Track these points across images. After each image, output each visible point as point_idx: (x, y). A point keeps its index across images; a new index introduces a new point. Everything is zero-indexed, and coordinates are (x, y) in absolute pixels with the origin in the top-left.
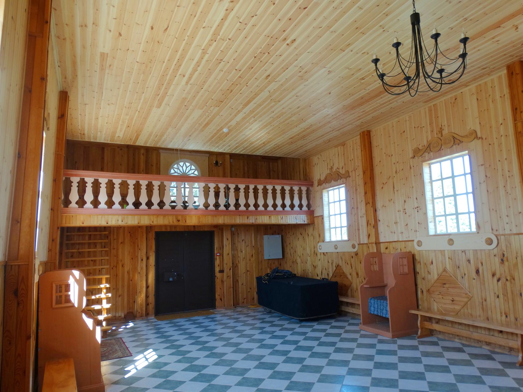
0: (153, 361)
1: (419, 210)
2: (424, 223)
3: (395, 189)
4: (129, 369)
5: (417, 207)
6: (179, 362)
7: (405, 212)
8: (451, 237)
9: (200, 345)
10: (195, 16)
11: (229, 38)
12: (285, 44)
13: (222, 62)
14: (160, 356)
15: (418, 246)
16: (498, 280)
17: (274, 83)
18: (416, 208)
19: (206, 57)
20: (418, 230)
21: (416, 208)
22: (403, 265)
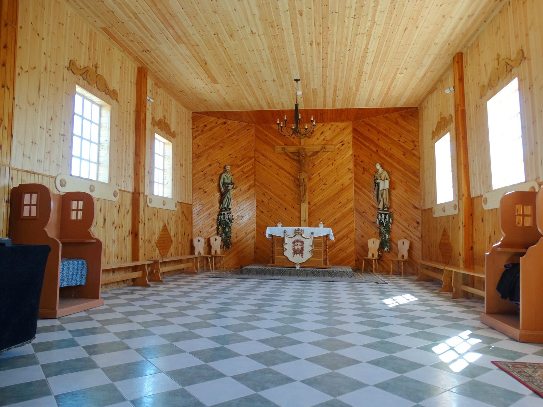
0: (438, 344)
1: (65, 139)
2: (67, 157)
3: (40, 92)
4: (472, 339)
5: (64, 135)
6: (393, 333)
7: (49, 134)
8: (93, 183)
9: (338, 340)
10: (387, 41)
11: (358, 36)
12: (314, 41)
13: (353, 16)
14: (428, 349)
15: (62, 186)
16: (115, 228)
17: (288, 9)
18: (62, 135)
19: (370, 17)
20: (61, 165)
21: (62, 135)
22: (523, 216)
